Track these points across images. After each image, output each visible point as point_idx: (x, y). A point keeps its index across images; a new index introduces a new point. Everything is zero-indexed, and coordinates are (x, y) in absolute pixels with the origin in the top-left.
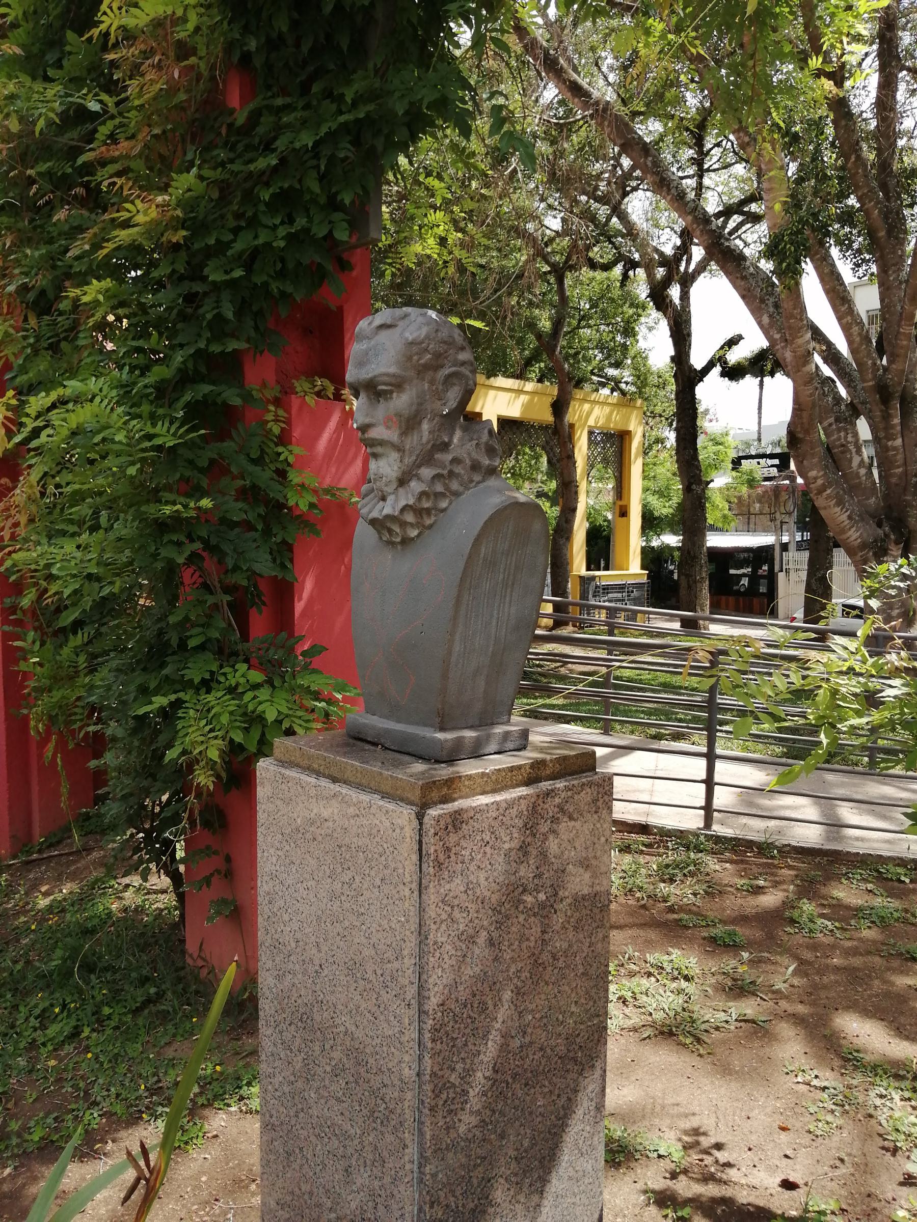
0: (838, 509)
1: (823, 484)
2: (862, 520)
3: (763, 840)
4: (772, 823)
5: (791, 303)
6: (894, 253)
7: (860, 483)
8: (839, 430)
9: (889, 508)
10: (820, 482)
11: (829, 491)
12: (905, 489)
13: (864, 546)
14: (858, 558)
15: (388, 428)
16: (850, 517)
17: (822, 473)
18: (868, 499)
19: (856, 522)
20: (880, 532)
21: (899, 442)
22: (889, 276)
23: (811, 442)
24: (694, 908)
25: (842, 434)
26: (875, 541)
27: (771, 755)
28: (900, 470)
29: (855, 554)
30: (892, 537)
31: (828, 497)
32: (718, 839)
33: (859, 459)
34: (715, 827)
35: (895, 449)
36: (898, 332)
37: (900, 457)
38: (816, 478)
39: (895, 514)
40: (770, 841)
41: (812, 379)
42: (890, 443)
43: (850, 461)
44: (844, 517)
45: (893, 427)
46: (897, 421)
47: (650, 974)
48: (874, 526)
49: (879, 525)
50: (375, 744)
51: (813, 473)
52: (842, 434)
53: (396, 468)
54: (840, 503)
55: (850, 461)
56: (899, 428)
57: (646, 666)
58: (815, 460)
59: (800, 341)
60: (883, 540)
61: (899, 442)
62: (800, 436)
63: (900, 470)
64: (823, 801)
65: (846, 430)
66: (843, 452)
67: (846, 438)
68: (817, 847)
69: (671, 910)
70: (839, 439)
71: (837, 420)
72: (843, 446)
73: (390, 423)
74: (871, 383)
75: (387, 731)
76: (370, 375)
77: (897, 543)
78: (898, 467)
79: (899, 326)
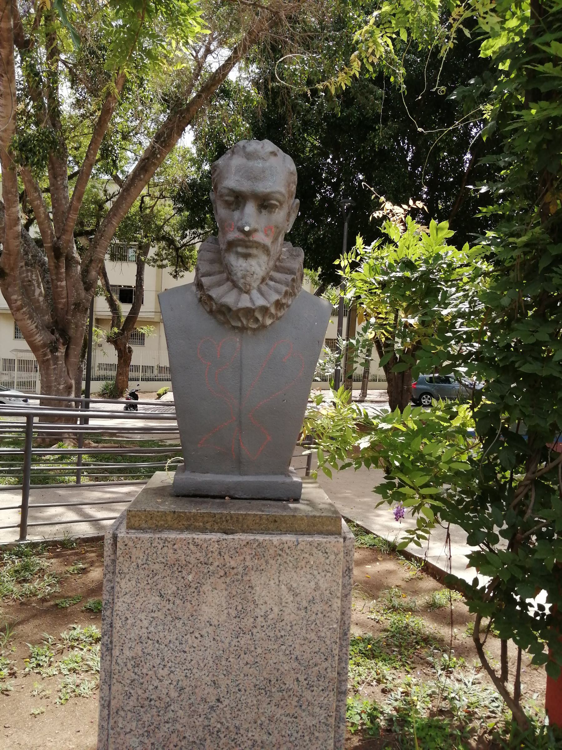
0: (29, 321)
1: (21, 305)
2: (43, 329)
3: (63, 538)
4: (57, 527)
5: (11, 184)
6: (61, 168)
7: (40, 306)
8: (27, 271)
9: (56, 323)
10: (19, 303)
11: (24, 309)
12: (67, 312)
13: (44, 345)
14: (40, 353)
15: (267, 235)
16: (36, 327)
17: (20, 297)
18: (44, 316)
19: (40, 330)
20: (54, 337)
21: (64, 283)
22: (57, 181)
23: (14, 276)
24: (56, 594)
25: (29, 274)
26: (51, 343)
27: (10, 484)
28: (65, 300)
29: (39, 350)
30: (61, 341)
31: (24, 313)
32: (34, 545)
33: (39, 290)
34: (28, 537)
35: (61, 287)
36: (68, 217)
37: (65, 292)
38: (16, 300)
39: (60, 327)
40: (68, 538)
41: (19, 236)
42: (59, 283)
43: (34, 291)
44: (33, 326)
45: (61, 273)
46: (63, 270)
47: (73, 647)
48: (50, 333)
49: (53, 333)
50: (223, 497)
51: (15, 297)
52: (29, 274)
53: (264, 269)
54: (31, 317)
55: (34, 291)
56: (64, 275)
57: (14, 430)
58: (16, 289)
59: (14, 210)
60: (55, 343)
61: (64, 283)
62: (7, 271)
63: (65, 300)
64: (71, 507)
65: (32, 272)
66: (30, 286)
67: (31, 276)
68: (96, 535)
69: (44, 600)
70: (27, 276)
71: (27, 264)
72: (30, 281)
73: (269, 232)
74: (49, 245)
75: (239, 483)
76: (268, 190)
77: (64, 345)
78: (63, 298)
79: (69, 213)
